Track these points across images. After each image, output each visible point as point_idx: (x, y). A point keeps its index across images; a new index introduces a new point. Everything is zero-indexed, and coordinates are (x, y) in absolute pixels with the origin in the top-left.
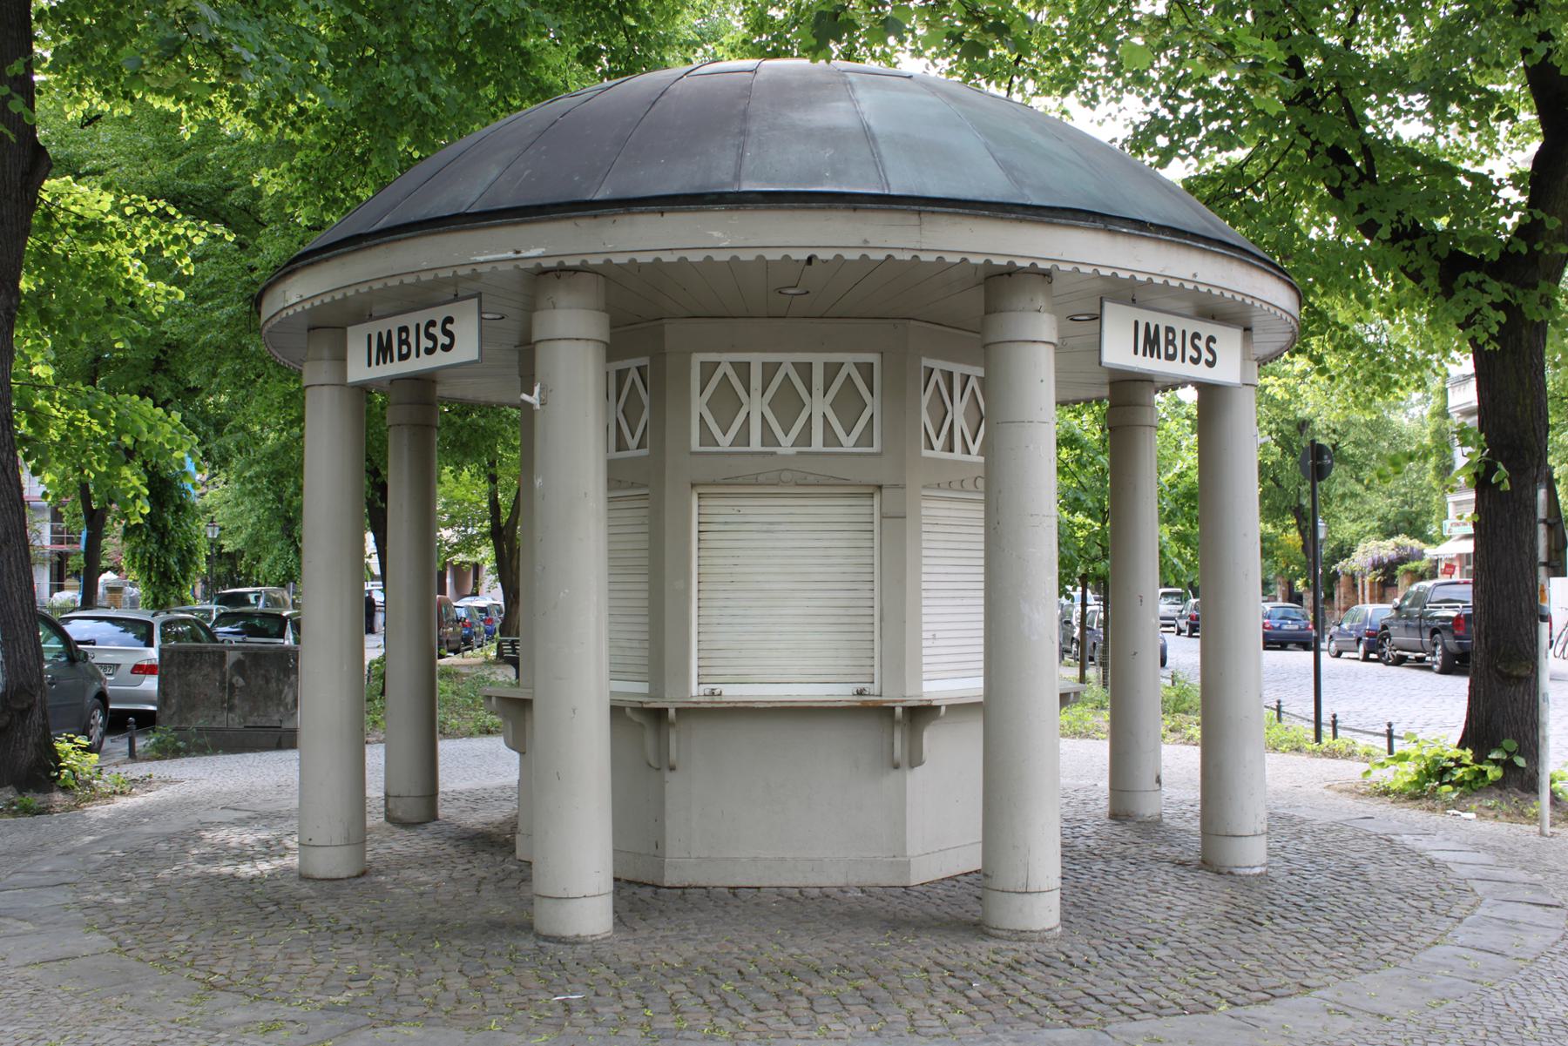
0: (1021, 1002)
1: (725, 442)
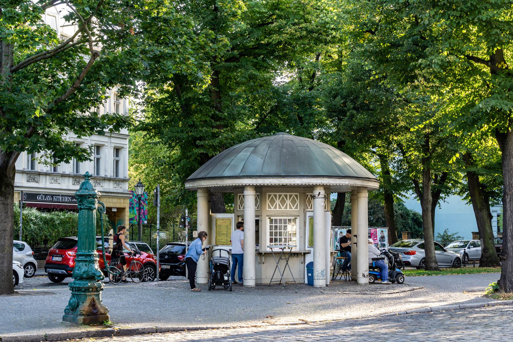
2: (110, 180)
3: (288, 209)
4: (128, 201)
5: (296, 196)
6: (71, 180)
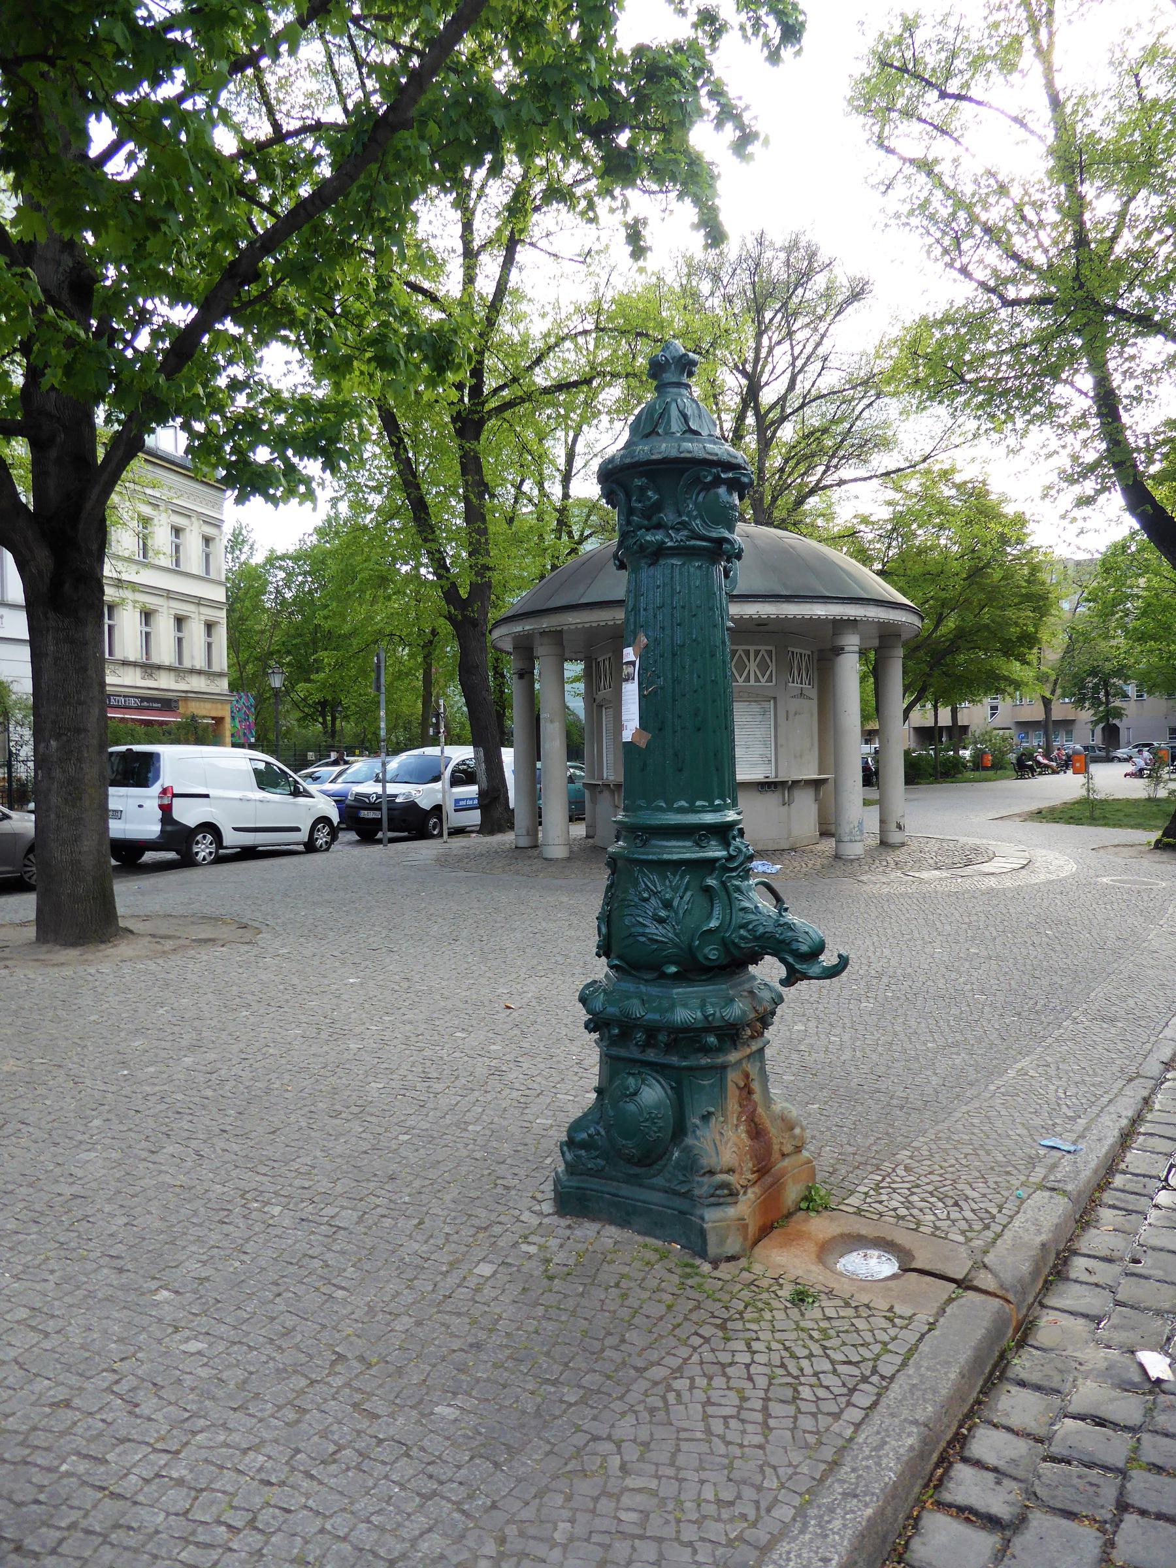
2: (200, 672)
3: (752, 682)
4: (228, 707)
5: (770, 653)
6: (138, 670)
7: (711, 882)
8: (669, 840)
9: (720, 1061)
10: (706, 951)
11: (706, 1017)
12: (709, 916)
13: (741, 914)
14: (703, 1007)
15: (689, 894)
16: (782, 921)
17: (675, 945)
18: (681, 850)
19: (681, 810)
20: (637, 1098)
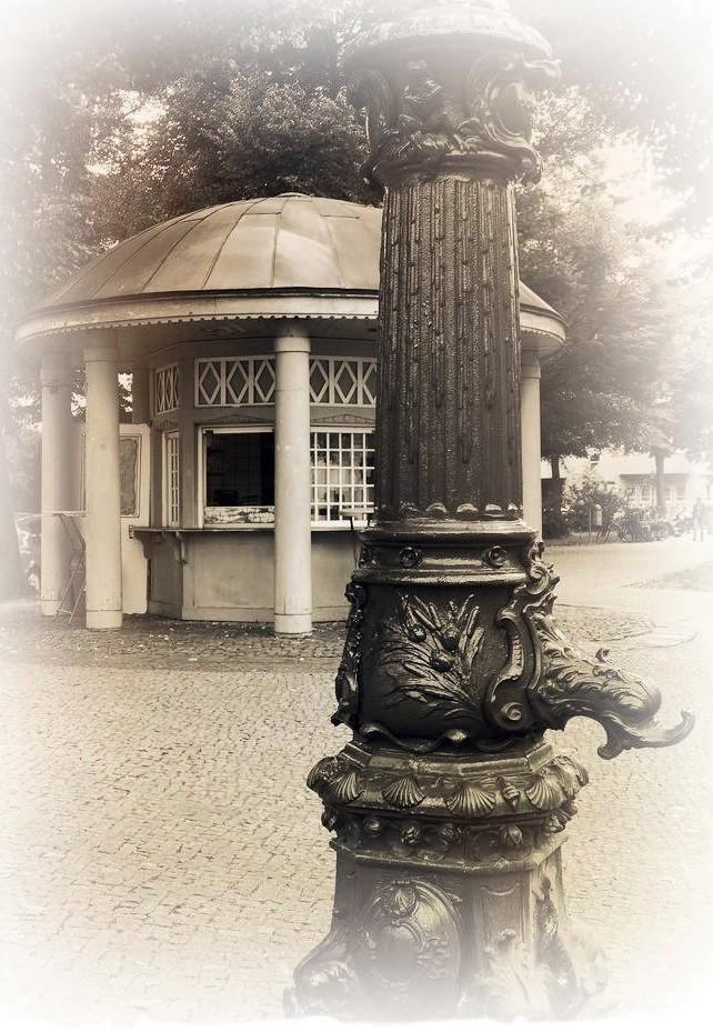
0: (79, 902)
1: (210, 402)
3: (332, 402)
7: (507, 614)
8: (443, 557)
9: (520, 863)
10: (505, 709)
11: (508, 802)
12: (508, 661)
13: (547, 659)
14: (501, 785)
15: (478, 633)
16: (604, 667)
17: (463, 702)
18: (461, 571)
19: (467, 517)
20: (411, 920)
